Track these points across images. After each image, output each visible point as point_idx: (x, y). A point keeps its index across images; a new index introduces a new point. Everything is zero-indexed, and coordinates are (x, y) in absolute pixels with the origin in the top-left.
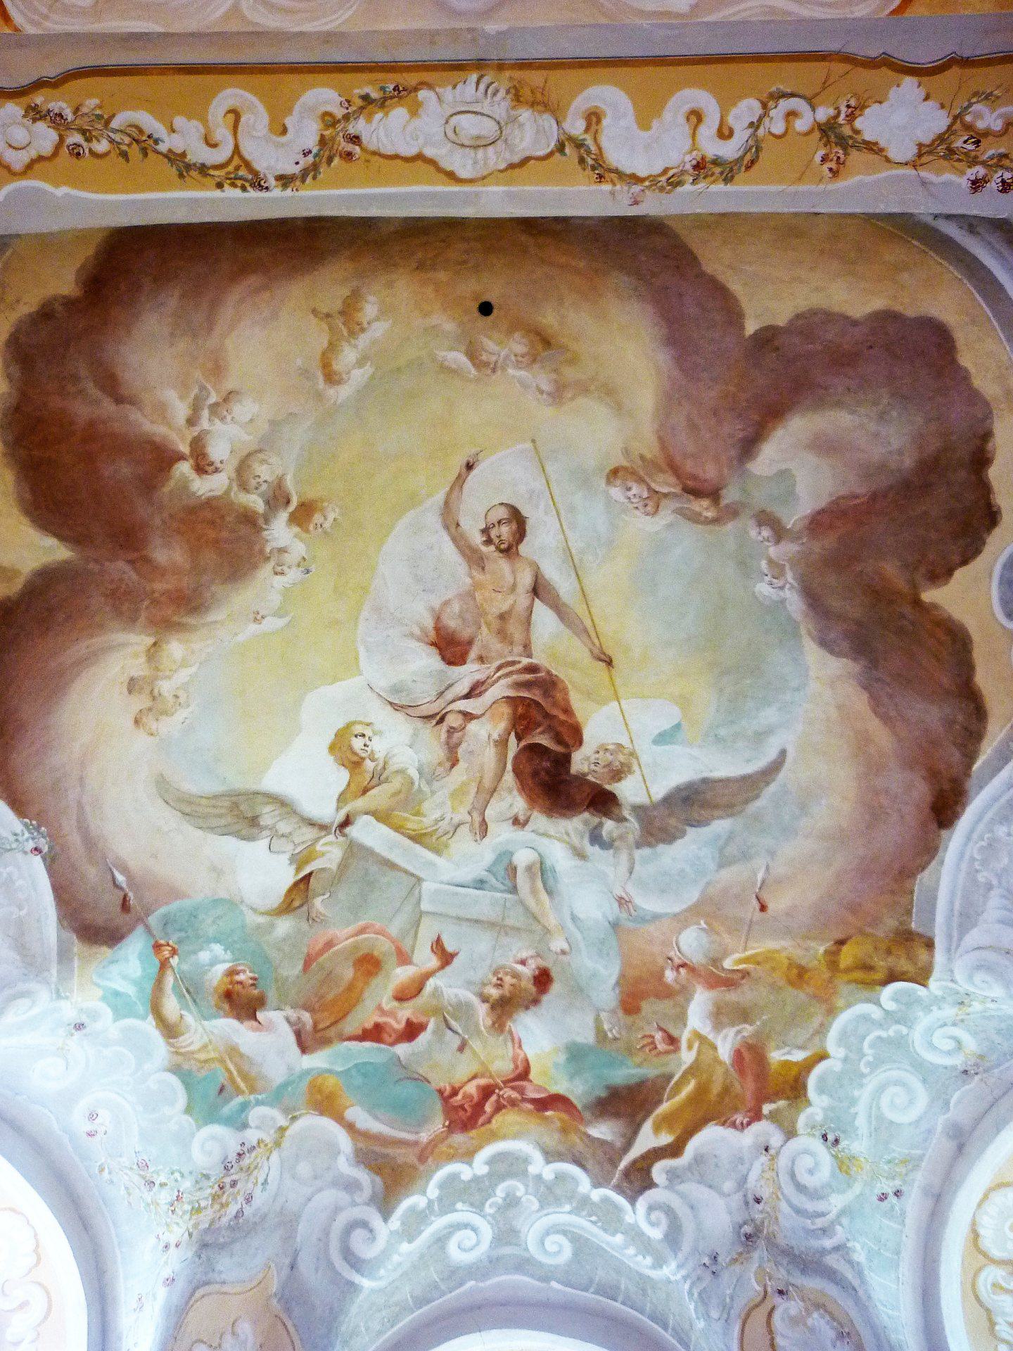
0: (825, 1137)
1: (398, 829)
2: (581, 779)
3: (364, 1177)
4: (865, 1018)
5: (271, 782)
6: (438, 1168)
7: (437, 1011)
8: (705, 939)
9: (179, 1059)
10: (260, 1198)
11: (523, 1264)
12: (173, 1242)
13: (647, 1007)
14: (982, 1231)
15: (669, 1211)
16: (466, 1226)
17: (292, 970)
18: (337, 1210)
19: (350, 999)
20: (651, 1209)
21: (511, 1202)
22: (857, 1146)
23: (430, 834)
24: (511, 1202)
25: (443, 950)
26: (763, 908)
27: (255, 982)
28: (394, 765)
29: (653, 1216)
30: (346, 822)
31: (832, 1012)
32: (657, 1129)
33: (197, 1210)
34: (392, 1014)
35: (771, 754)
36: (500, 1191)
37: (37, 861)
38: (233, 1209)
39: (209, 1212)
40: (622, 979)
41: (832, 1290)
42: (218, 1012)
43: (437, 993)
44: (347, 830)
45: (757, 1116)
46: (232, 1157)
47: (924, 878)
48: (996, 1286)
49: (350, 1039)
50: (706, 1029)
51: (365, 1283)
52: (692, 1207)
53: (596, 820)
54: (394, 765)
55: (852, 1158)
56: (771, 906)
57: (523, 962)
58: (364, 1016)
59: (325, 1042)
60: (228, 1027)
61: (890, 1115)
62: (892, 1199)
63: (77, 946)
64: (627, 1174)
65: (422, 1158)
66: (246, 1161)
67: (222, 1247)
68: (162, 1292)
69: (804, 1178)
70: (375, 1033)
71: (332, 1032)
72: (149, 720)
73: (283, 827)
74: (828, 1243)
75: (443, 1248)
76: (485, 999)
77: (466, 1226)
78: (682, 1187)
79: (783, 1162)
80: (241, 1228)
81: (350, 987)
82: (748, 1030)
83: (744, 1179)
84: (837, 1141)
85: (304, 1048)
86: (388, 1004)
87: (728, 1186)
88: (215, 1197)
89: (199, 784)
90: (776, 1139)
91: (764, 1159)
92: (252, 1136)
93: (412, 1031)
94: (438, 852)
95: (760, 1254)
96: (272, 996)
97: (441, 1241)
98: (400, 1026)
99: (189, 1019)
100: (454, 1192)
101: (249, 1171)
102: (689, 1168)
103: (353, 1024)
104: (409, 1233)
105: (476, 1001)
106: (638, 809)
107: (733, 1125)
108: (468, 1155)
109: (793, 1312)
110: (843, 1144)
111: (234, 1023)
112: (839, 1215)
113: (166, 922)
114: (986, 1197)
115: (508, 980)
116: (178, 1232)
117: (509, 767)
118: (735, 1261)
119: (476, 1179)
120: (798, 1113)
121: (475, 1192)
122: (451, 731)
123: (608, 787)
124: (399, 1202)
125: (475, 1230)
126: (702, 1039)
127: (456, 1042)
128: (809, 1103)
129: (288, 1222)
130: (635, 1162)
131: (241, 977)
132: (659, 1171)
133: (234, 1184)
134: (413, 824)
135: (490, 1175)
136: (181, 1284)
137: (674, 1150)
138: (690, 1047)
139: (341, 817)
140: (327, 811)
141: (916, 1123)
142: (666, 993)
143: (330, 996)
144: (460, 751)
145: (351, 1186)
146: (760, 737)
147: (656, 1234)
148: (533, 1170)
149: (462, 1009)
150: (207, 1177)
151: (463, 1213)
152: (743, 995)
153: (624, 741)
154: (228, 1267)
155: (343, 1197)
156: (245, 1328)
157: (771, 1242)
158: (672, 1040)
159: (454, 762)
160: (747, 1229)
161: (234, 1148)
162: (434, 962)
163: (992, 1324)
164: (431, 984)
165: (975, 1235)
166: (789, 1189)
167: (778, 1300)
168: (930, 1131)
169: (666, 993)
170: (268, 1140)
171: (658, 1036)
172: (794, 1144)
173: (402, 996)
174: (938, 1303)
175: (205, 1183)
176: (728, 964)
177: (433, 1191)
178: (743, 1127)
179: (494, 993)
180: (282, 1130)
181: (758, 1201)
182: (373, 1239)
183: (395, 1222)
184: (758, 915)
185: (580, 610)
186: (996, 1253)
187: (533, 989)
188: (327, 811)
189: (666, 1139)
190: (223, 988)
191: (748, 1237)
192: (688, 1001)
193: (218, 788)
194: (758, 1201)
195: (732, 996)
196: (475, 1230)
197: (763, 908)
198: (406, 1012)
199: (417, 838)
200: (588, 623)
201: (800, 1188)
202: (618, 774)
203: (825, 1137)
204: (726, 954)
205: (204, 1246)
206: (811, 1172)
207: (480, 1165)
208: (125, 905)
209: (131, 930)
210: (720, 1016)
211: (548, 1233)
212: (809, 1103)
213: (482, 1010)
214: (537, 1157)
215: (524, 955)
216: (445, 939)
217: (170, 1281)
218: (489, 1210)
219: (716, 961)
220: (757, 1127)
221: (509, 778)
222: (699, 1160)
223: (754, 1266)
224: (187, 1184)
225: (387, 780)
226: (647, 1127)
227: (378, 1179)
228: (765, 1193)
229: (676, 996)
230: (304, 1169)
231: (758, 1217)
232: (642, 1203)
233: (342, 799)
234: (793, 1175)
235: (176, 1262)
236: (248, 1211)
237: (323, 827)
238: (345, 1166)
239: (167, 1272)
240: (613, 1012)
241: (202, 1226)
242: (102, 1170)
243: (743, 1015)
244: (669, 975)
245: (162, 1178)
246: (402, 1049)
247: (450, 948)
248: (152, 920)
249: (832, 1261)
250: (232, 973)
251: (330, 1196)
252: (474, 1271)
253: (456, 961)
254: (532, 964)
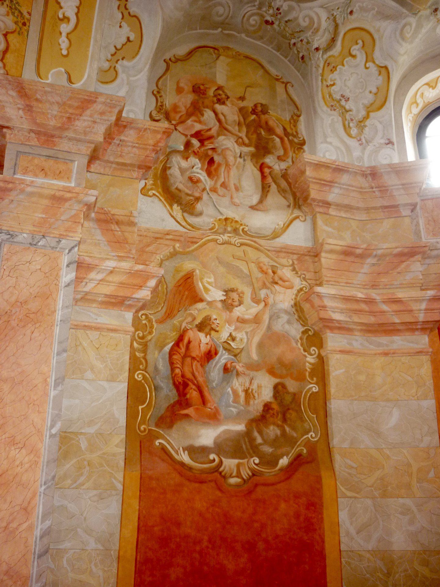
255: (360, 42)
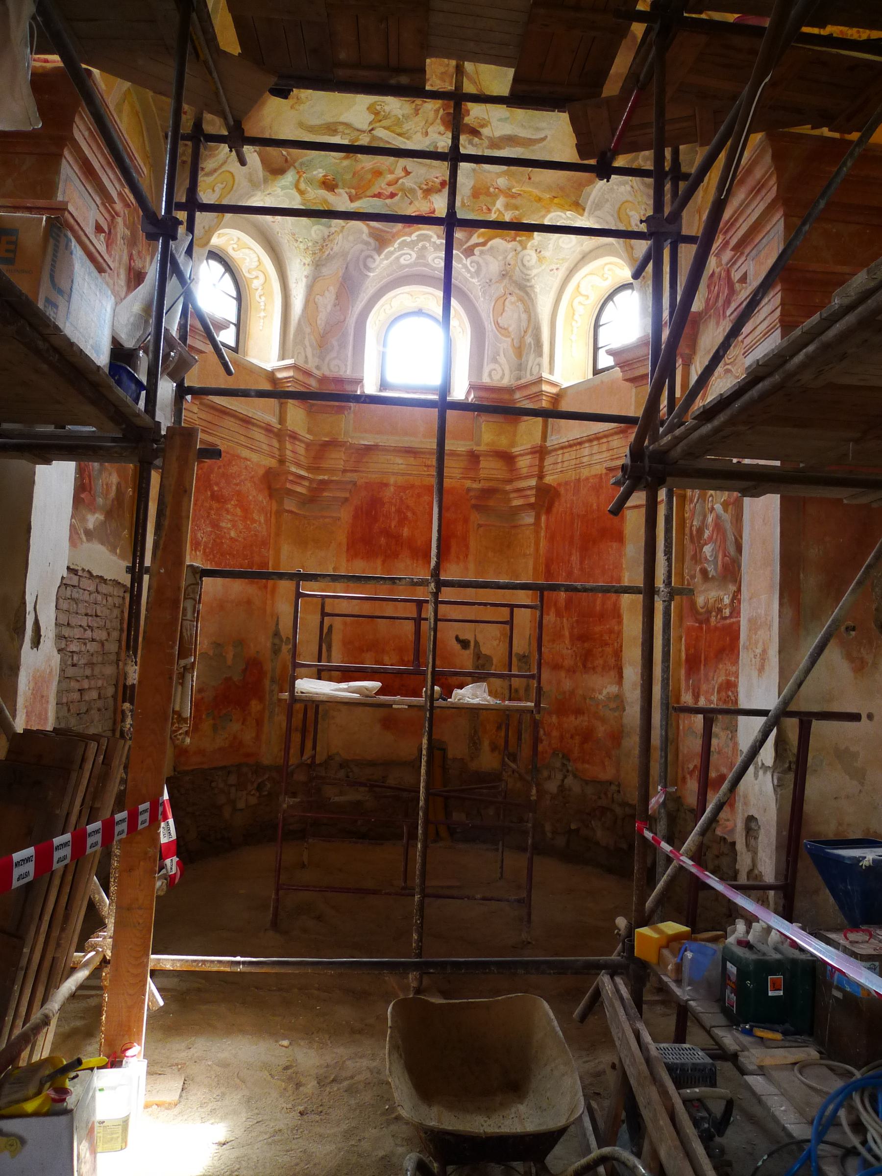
0: (536, 250)
1: (393, 132)
2: (467, 125)
3: (371, 241)
4: (561, 216)
5: (343, 119)
6: (399, 239)
7: (402, 189)
8: (506, 182)
9: (306, 202)
10: (336, 249)
11: (427, 265)
12: (307, 263)
13: (482, 197)
14: (581, 286)
15: (478, 263)
16: (407, 254)
17: (348, 177)
18: (362, 251)
19: (370, 184)
20: (471, 263)
21: (424, 248)
22: (546, 254)
23: (405, 134)
24: (424, 248)
25: (407, 170)
26: (530, 178)
27: (334, 179)
28: (392, 114)
29: (473, 264)
30: (372, 129)
31: (548, 212)
32: (478, 237)
33: (314, 254)
34: (385, 189)
35: (541, 135)
36: (420, 245)
37: (255, 154)
38: (327, 253)
39: (319, 254)
40: (474, 187)
41: (526, 298)
42: (320, 187)
43: (403, 183)
44: (373, 132)
45: (514, 240)
46: (326, 237)
47: (588, 189)
48: (580, 303)
49: (369, 197)
50: (502, 209)
51: (372, 274)
52: (487, 263)
53: (471, 137)
54: (392, 114)
55: (544, 257)
56: (532, 179)
57: (437, 178)
58: (375, 190)
59: (360, 198)
60: (323, 193)
61: (561, 244)
62: (555, 271)
63: (270, 177)
64: (465, 250)
65: (393, 237)
66: (331, 237)
67: (323, 265)
68: (304, 280)
69: (526, 263)
70: (378, 195)
71: (362, 195)
72: (297, 107)
73: (346, 131)
74: (528, 284)
75: (398, 260)
76: (421, 189)
77: (407, 254)
78: (485, 256)
79: (520, 256)
80: (330, 258)
81: (370, 181)
82: (517, 212)
83: (506, 258)
84: (540, 252)
85: (352, 200)
86: (383, 185)
87: (500, 258)
88: (321, 250)
89: (461, 637)
90: (519, 248)
91: (514, 253)
92: (333, 230)
93: (392, 195)
94: (408, 139)
95: (506, 281)
96: (340, 184)
97: (398, 258)
98: (388, 193)
99: (309, 189)
100: (404, 244)
101: (331, 241)
102: (488, 250)
103: (369, 193)
104: (387, 258)
105: (417, 188)
106: (488, 137)
107: (506, 240)
108: (410, 234)
109: (513, 300)
110: (542, 253)
111: (327, 192)
112: (535, 276)
113: (302, 164)
114: (585, 276)
115: (430, 183)
116: (308, 260)
117: (439, 118)
118: (497, 282)
119: (412, 241)
120: (529, 241)
121: (411, 245)
122: (417, 105)
123: (479, 129)
124: (384, 250)
125: (410, 255)
126: (500, 212)
127: (409, 201)
128: (533, 239)
129: (344, 254)
130: (469, 247)
131: (329, 177)
132: (477, 251)
133: (327, 245)
134: (399, 131)
135: (417, 240)
136: (311, 278)
137: (484, 244)
138: (495, 213)
139: (370, 128)
140: (365, 127)
141: (570, 248)
142: (488, 194)
143: (362, 184)
144: (420, 112)
145: (367, 243)
146: (538, 129)
147: (473, 270)
148: (432, 240)
149: (412, 191)
150: (317, 243)
151: (406, 250)
152: (518, 201)
153: (486, 118)
154: (325, 271)
155: (365, 247)
156: (331, 288)
157: (511, 278)
158: (489, 210)
159: (417, 114)
160: (504, 273)
161: (326, 233)
162: (403, 174)
163: (574, 314)
164: (401, 181)
165: (578, 286)
166: (520, 264)
167: (509, 296)
168: (574, 252)
169: (488, 194)
170: (338, 230)
171: (484, 207)
172: (525, 252)
173: (389, 184)
174: (569, 282)
175: (317, 245)
176: (513, 190)
177: (396, 245)
178: (509, 241)
179: (425, 187)
180: (344, 227)
181: (509, 265)
182: (374, 262)
183: (382, 256)
184: (527, 180)
185: (475, 76)
186: (583, 292)
187: (440, 187)
188: (365, 127)
189: (481, 240)
190: (322, 180)
191: (503, 275)
192: (497, 199)
193: (323, 122)
194: (509, 265)
195: (513, 201)
196: (410, 255)
197: (530, 178)
198: (391, 189)
199: (399, 135)
200: (477, 82)
201: (524, 265)
202: (482, 126)
203: (536, 250)
204: (514, 187)
205: (317, 266)
206: (528, 261)
207: (414, 237)
208: (286, 160)
209: (289, 168)
210: (507, 206)
211: (436, 258)
212: (533, 239)
213: (420, 193)
214: (435, 237)
215: (438, 175)
216: (407, 167)
217: (307, 277)
218: (415, 249)
219: (509, 189)
220: (513, 243)
221: (439, 121)
222: (491, 248)
223: (503, 285)
224: (310, 244)
225: (389, 118)
226: (475, 235)
227: (377, 243)
228: (512, 263)
229: (495, 197)
230: (351, 238)
231: (508, 269)
232: (469, 260)
233: (370, 123)
234: (522, 261)
235: (307, 271)
236: (331, 253)
237: (364, 132)
238: (365, 237)
239: (305, 273)
240: (469, 197)
241: (317, 259)
242: (278, 233)
243: (516, 208)
244: (492, 190)
245: (301, 240)
246: (388, 201)
247: (409, 170)
248: (296, 164)
249: (528, 289)
250: (324, 176)
251: (360, 246)
252: (407, 266)
253: (411, 175)
254: (440, 179)
255: (225, 183)
